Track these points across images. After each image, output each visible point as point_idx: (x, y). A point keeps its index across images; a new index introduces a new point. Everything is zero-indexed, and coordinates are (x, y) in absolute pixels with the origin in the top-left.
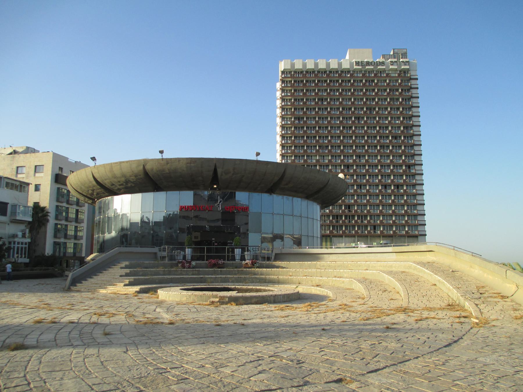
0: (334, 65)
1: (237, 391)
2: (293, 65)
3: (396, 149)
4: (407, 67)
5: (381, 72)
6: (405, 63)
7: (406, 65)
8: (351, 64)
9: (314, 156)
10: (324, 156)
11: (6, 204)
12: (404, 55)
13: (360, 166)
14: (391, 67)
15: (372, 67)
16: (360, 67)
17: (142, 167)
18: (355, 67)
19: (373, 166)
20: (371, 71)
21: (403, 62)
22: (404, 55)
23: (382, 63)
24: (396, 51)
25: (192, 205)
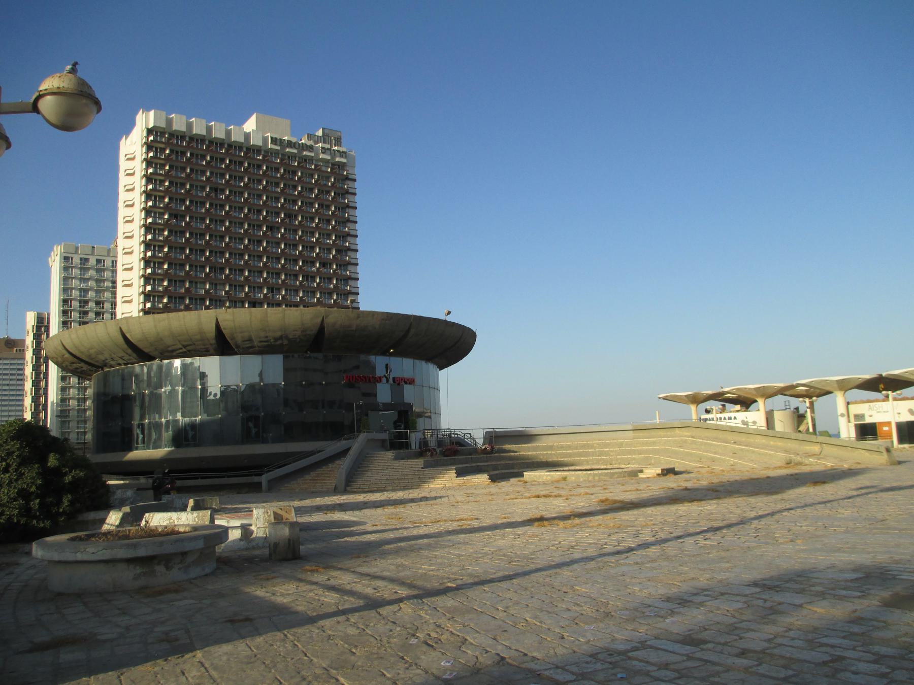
0: (218, 132)
1: (194, 673)
2: (169, 122)
3: (235, 274)
4: (344, 160)
5: (309, 160)
6: (343, 154)
7: (342, 157)
8: (265, 140)
9: (201, 283)
10: (216, 285)
11: (856, 425)
12: (338, 141)
13: (175, 298)
14: (321, 156)
15: (295, 151)
16: (278, 148)
17: (320, 320)
18: (270, 146)
19: (196, 299)
20: (292, 157)
21: (338, 151)
22: (338, 141)
23: (310, 148)
24: (326, 131)
25: (378, 385)
